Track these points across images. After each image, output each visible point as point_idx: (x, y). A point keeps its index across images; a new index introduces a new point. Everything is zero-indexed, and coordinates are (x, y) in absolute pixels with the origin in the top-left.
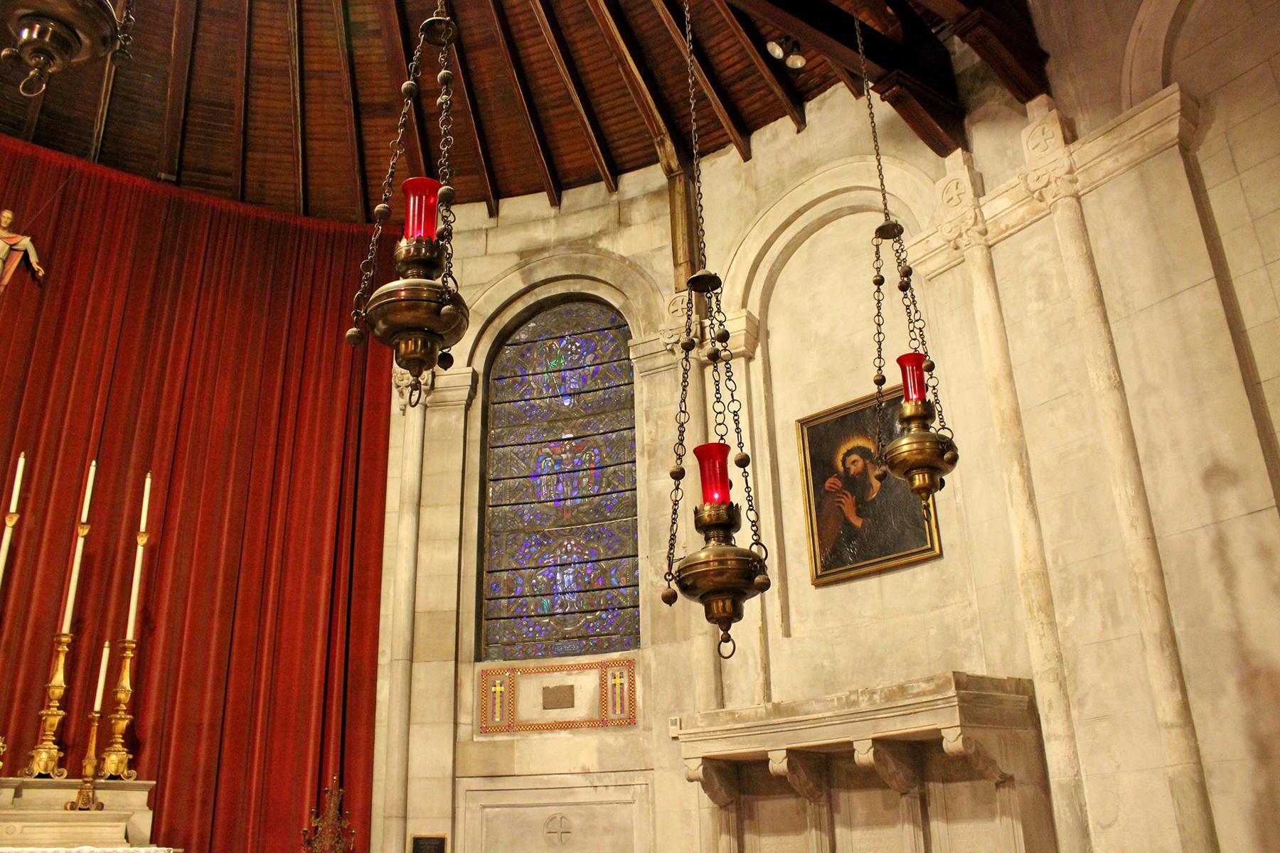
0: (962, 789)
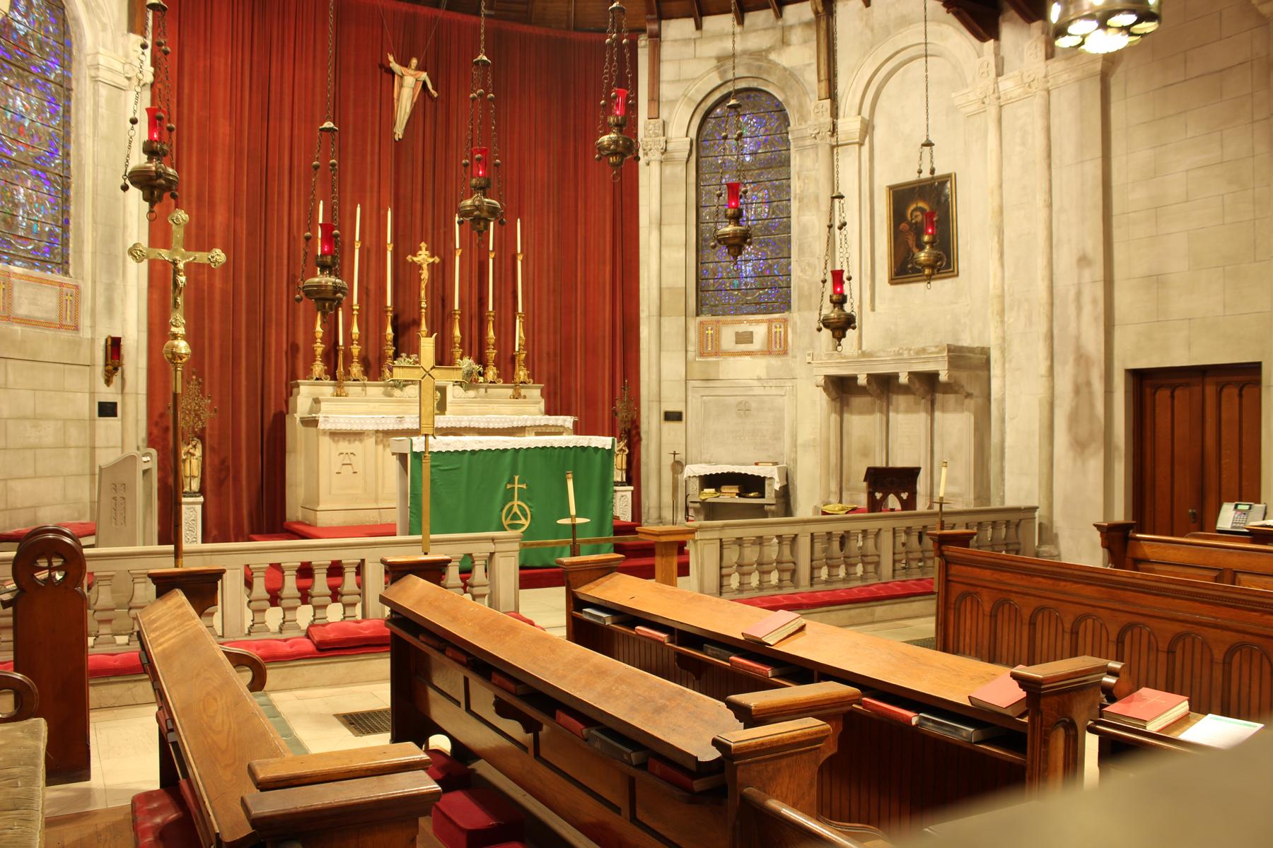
0: (951, 398)
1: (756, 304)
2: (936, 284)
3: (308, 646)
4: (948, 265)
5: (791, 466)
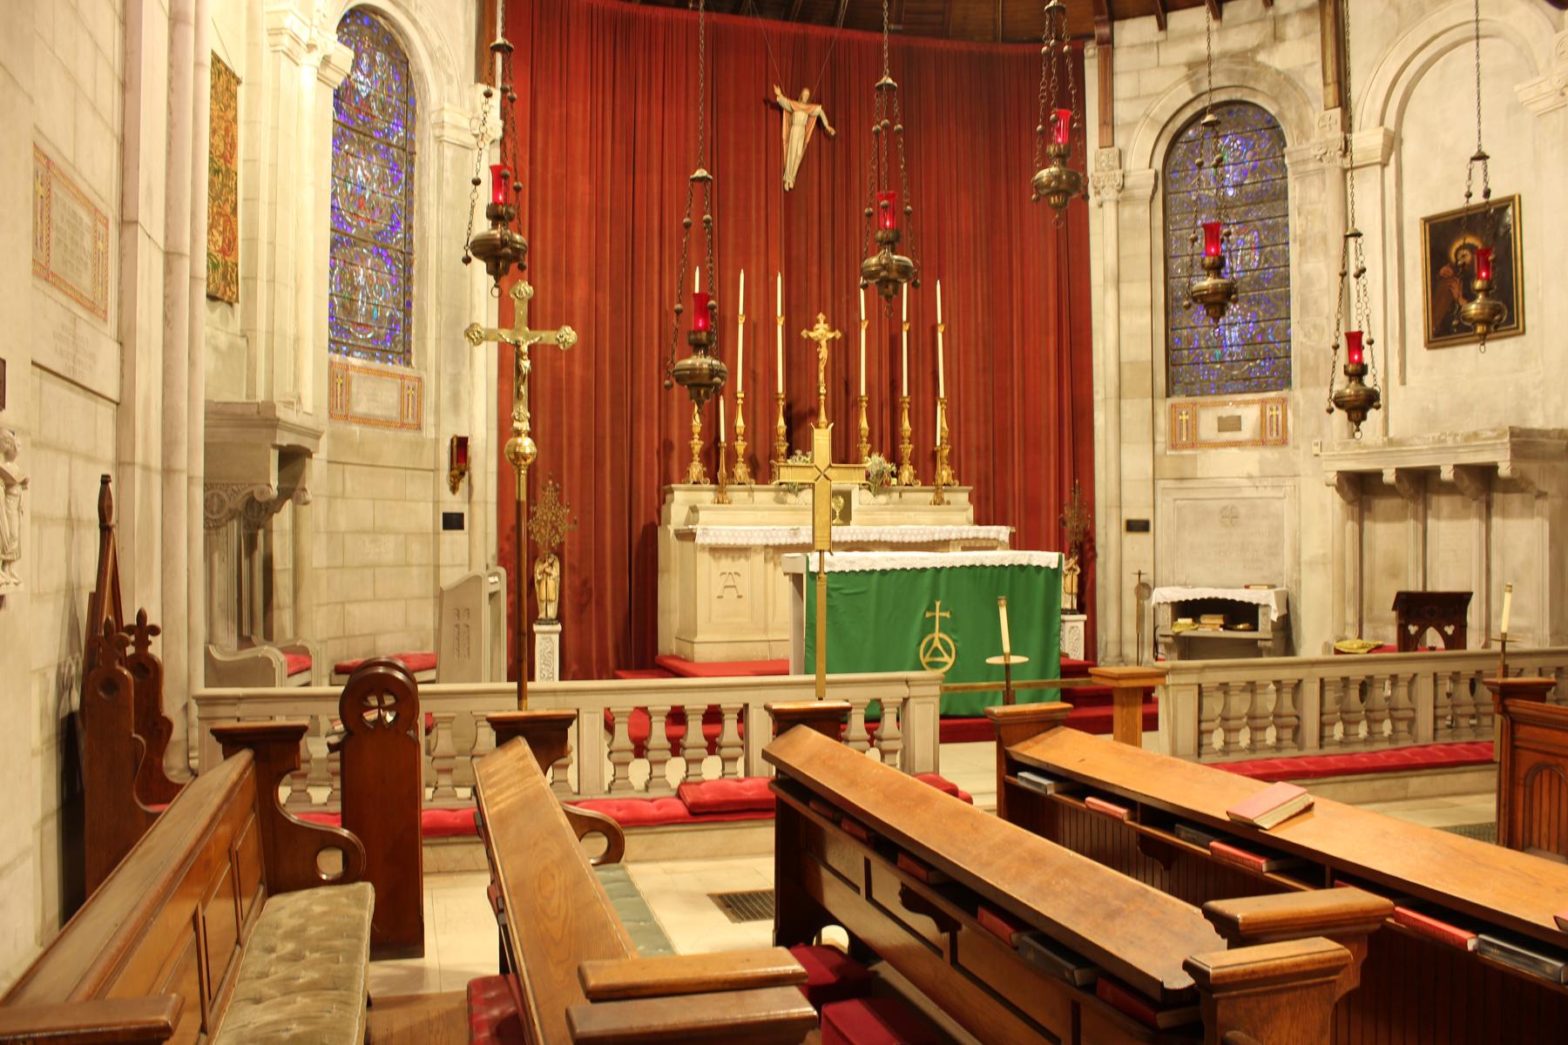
0: (1515, 499)
1: (1245, 380)
2: (1490, 345)
3: (679, 809)
4: (1510, 320)
5: (1294, 589)
